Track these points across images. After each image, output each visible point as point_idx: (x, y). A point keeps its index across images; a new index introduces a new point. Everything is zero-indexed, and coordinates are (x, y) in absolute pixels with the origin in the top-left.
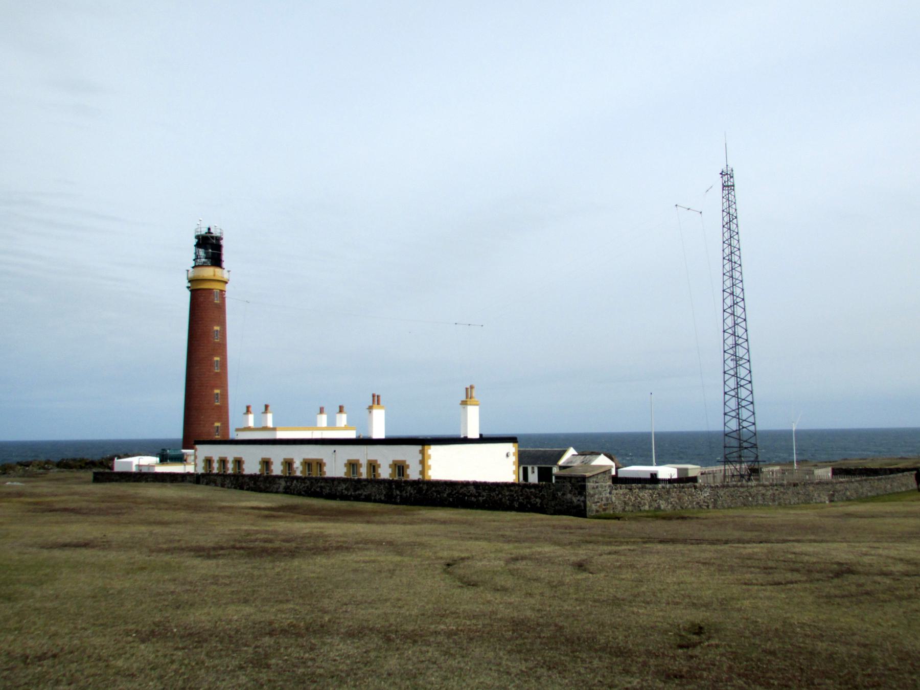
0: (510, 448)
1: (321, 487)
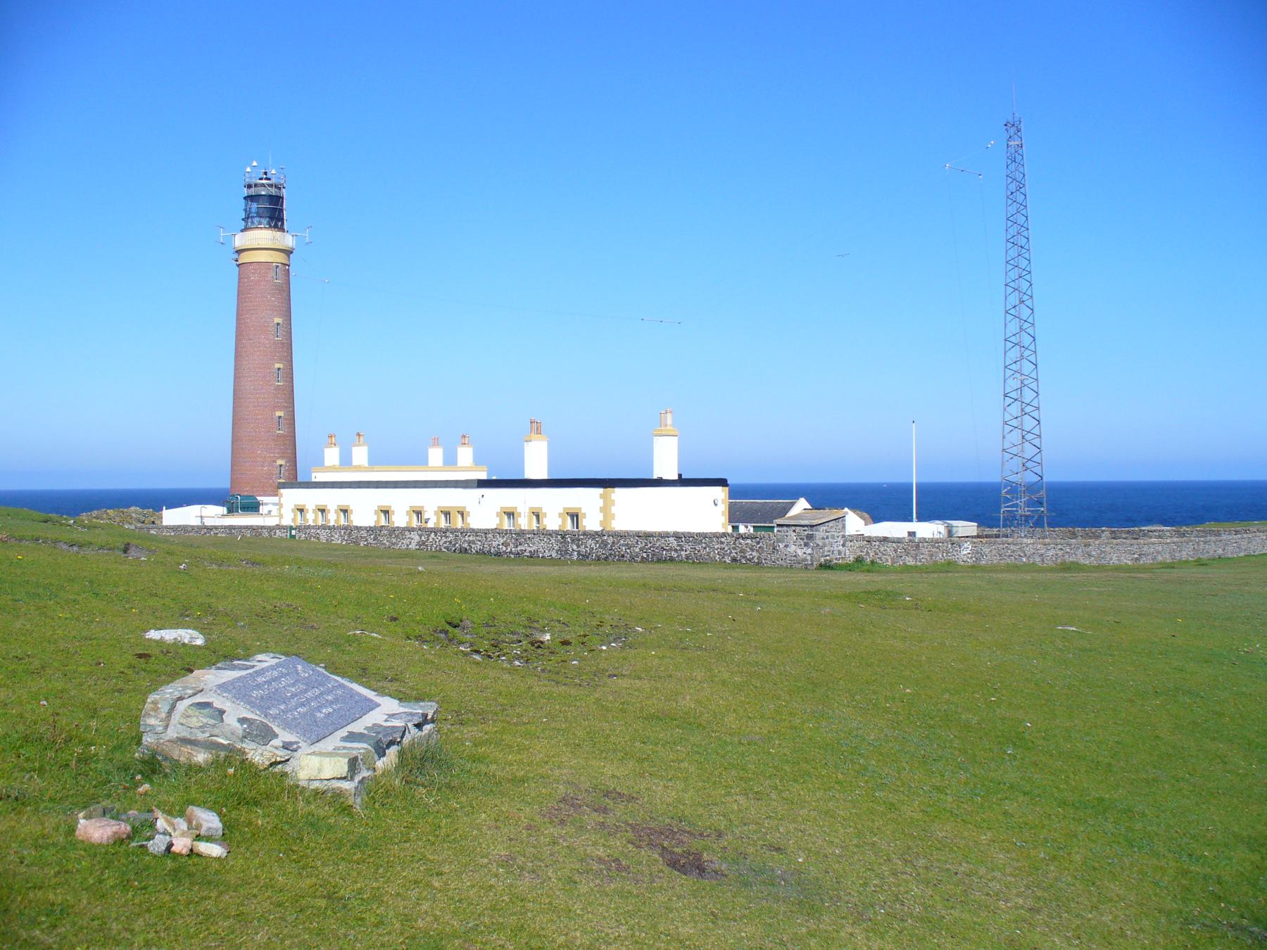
0: (719, 493)
1: (469, 542)
